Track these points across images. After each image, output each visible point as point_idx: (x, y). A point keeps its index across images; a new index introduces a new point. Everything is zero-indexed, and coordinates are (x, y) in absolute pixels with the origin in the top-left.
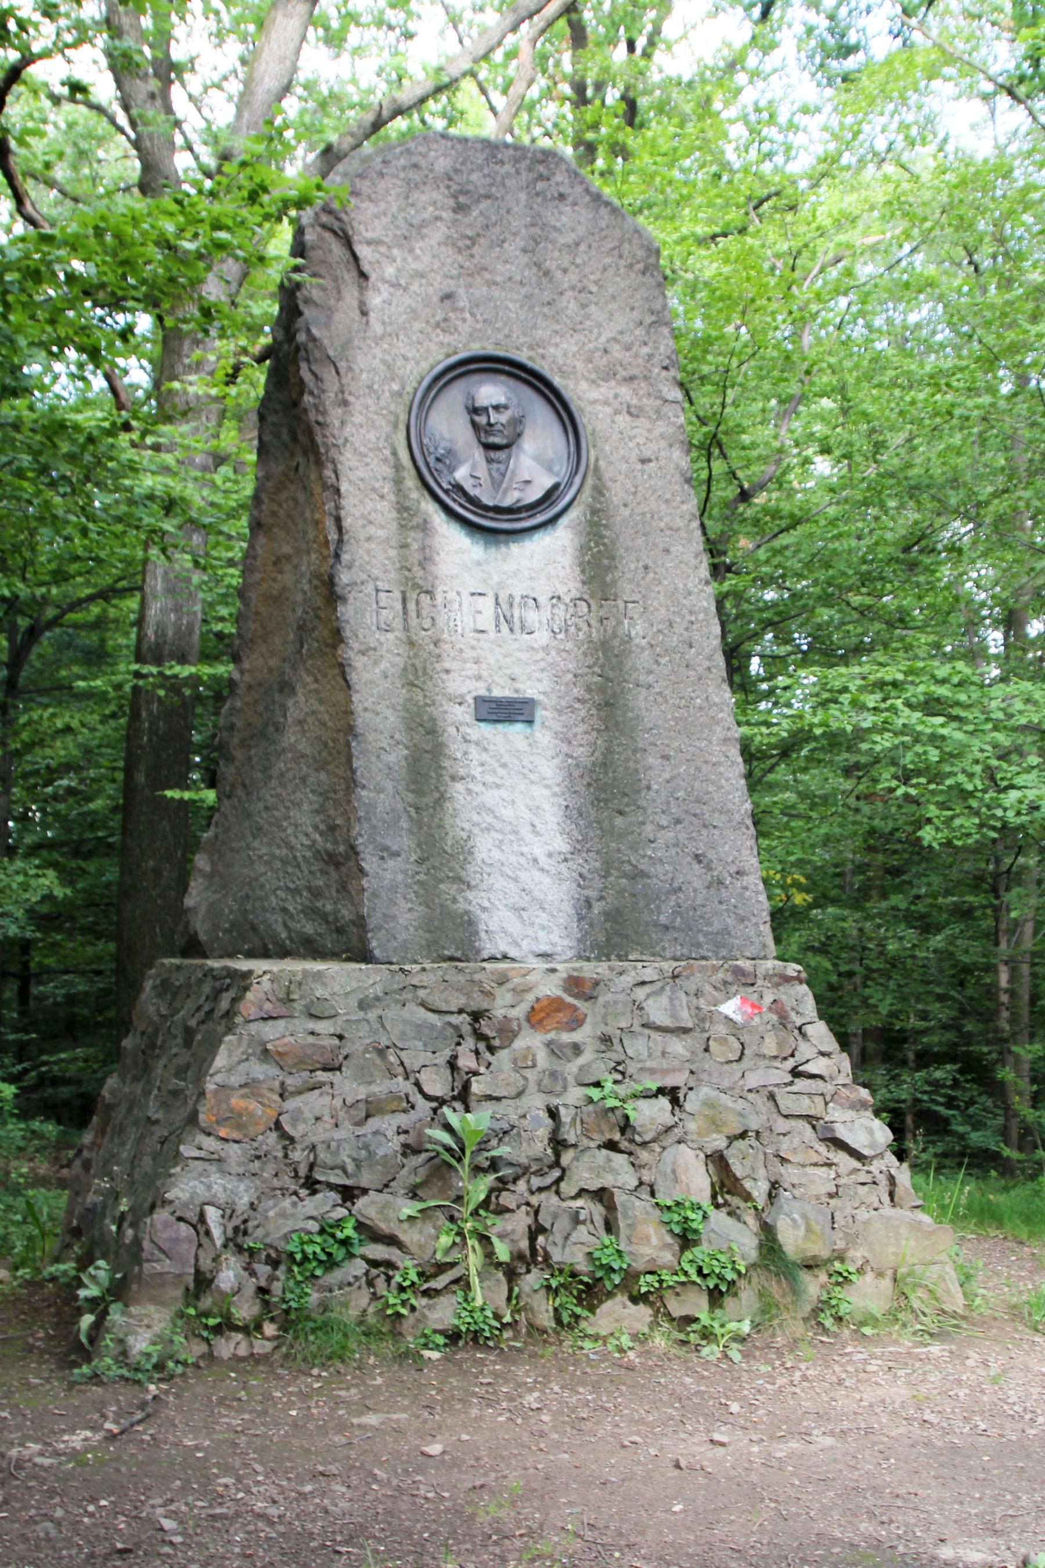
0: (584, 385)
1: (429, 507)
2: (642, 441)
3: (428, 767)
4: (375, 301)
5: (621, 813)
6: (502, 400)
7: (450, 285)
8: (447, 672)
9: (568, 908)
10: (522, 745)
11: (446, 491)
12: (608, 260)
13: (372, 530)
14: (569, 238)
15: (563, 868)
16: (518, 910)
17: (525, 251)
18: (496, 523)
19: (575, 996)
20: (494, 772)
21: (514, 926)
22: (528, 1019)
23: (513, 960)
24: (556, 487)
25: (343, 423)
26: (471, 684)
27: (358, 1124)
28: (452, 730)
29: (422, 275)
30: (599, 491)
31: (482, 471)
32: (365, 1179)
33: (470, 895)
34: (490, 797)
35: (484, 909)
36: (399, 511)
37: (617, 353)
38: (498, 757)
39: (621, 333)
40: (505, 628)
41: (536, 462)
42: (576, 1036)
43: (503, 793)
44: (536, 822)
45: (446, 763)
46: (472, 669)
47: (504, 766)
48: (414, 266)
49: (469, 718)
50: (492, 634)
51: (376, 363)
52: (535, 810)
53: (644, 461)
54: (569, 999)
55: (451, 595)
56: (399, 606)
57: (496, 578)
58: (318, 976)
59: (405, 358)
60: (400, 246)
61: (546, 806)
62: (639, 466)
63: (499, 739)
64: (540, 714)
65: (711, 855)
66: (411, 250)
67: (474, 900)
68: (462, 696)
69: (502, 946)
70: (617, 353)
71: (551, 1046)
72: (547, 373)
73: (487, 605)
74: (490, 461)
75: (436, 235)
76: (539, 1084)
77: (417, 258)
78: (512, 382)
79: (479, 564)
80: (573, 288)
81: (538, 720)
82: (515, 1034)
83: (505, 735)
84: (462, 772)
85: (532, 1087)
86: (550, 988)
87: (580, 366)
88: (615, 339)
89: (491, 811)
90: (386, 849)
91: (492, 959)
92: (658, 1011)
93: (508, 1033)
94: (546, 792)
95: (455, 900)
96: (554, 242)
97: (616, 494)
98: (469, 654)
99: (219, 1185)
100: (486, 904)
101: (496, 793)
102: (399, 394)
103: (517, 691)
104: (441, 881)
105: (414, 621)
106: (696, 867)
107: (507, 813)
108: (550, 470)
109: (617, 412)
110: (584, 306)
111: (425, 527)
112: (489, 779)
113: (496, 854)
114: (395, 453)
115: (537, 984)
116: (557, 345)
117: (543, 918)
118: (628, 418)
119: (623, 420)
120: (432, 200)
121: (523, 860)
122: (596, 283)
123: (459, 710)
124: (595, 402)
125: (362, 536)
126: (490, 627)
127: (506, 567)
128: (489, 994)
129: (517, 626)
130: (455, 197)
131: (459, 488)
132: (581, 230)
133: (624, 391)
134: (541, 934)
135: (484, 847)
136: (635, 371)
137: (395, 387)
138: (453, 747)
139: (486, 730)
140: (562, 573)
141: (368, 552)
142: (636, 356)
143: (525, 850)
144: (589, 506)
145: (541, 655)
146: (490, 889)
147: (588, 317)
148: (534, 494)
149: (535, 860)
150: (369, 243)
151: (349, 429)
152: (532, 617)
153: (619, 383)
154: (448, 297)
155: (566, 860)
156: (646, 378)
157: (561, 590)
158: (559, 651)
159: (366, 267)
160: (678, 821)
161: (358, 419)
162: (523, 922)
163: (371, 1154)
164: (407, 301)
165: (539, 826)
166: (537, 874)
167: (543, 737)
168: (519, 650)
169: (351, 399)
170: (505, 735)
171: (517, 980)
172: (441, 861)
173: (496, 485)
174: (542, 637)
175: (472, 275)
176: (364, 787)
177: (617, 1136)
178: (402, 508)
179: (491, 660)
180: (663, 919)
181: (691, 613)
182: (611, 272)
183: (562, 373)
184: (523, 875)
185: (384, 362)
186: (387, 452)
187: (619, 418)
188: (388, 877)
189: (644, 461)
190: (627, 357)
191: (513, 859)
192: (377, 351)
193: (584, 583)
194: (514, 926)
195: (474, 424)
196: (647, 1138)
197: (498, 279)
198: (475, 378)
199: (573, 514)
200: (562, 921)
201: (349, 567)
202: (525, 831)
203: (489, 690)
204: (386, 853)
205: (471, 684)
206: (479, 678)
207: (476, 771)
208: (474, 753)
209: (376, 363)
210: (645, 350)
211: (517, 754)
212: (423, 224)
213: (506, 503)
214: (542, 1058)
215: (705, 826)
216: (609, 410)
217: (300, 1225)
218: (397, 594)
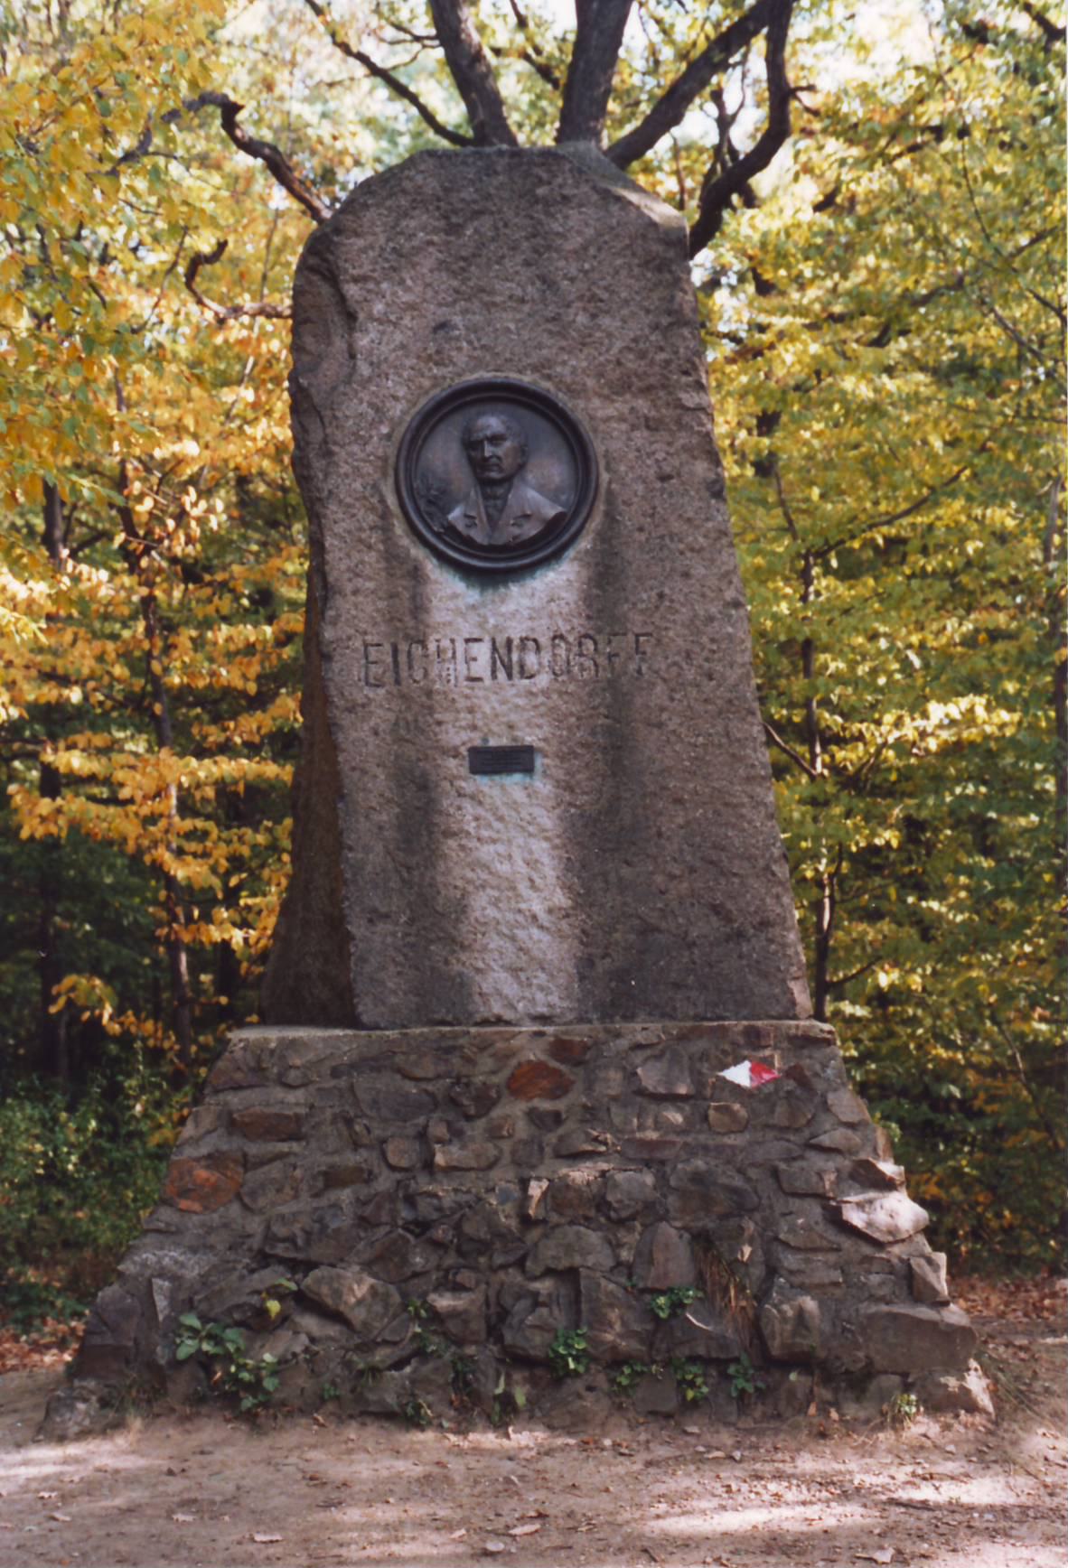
0: (596, 402)
1: (418, 552)
2: (660, 456)
3: (421, 823)
4: (363, 341)
5: (628, 863)
7: (443, 313)
8: (439, 723)
9: (570, 967)
10: (519, 795)
11: (438, 535)
12: (619, 262)
13: (359, 582)
14: (575, 242)
15: (564, 925)
16: (515, 971)
17: (527, 263)
18: (494, 565)
19: (562, 1061)
20: (490, 826)
21: (510, 988)
22: (508, 1086)
23: (508, 1023)
25: (326, 475)
26: (464, 736)
27: (316, 1195)
28: (446, 785)
29: (412, 307)
31: (479, 511)
32: (315, 1253)
33: (463, 957)
34: (486, 852)
35: (478, 971)
36: (387, 560)
37: (631, 363)
38: (494, 810)
39: (635, 340)
40: (502, 675)
41: (537, 496)
42: (560, 1105)
43: (501, 848)
44: (535, 876)
45: (437, 819)
46: (465, 718)
47: (501, 819)
48: (406, 298)
49: (464, 771)
50: (488, 682)
51: (364, 407)
52: (532, 863)
53: (664, 478)
54: (554, 1064)
55: (446, 643)
56: (389, 660)
57: (492, 621)
58: (293, 1043)
59: (395, 398)
60: (390, 279)
61: (546, 860)
62: (658, 485)
63: (496, 792)
64: (539, 762)
65: (730, 905)
66: (402, 282)
67: (463, 963)
68: (456, 748)
69: (497, 1008)
70: (631, 363)
71: (533, 1116)
73: (482, 651)
74: (486, 497)
75: (427, 263)
76: (513, 1153)
77: (408, 290)
79: (473, 607)
80: (581, 298)
82: (494, 1103)
83: (503, 787)
84: (455, 827)
85: (507, 1158)
86: (535, 1053)
87: (590, 382)
88: (629, 349)
89: (486, 867)
90: (375, 911)
91: (485, 1022)
92: (650, 1076)
93: (485, 1101)
94: (545, 845)
95: (447, 962)
96: (558, 250)
97: (630, 518)
99: (171, 1256)
100: (480, 965)
101: (492, 848)
102: (389, 437)
104: (432, 942)
105: (404, 674)
106: (714, 919)
107: (504, 868)
108: (555, 499)
109: (634, 427)
110: (594, 316)
111: (416, 574)
112: (485, 833)
113: (491, 912)
114: (382, 501)
115: (522, 1048)
116: (564, 363)
117: (542, 978)
118: (646, 433)
120: (420, 225)
121: (520, 918)
122: (606, 289)
123: (452, 763)
124: (608, 419)
125: (349, 587)
126: (486, 674)
127: (503, 609)
128: (470, 1061)
129: (516, 669)
130: (446, 218)
131: (451, 529)
132: (590, 232)
133: (642, 405)
134: (540, 996)
135: (481, 906)
136: (652, 380)
137: (385, 430)
138: (445, 803)
139: (483, 783)
140: (565, 610)
141: (356, 606)
142: (652, 363)
143: (523, 906)
145: (541, 699)
146: (485, 949)
148: (531, 530)
149: (534, 917)
150: (356, 280)
151: (332, 481)
152: (531, 659)
153: (635, 396)
154: (443, 326)
155: (567, 916)
156: (664, 387)
157: (564, 628)
158: (561, 693)
159: (353, 306)
160: (692, 870)
161: (345, 468)
162: (520, 983)
163: (324, 1228)
164: (398, 337)
165: (538, 881)
166: (535, 932)
167: (543, 786)
168: (518, 695)
169: (336, 449)
170: (503, 787)
171: (500, 1045)
172: (435, 921)
173: (493, 522)
174: (543, 680)
175: (468, 300)
176: (351, 849)
177: (592, 1213)
178: (392, 556)
179: (487, 710)
181: (713, 640)
182: (624, 273)
183: (571, 391)
184: (520, 934)
185: (371, 404)
186: (374, 500)
187: (637, 434)
188: (375, 941)
189: (664, 478)
190: (641, 366)
191: (510, 916)
192: (365, 396)
193: (589, 617)
194: (510, 988)
196: (624, 1214)
197: (498, 299)
200: (562, 980)
201: (334, 623)
202: (523, 888)
203: (485, 740)
204: (375, 917)
205: (464, 736)
206: (474, 728)
207: (471, 827)
208: (469, 807)
209: (364, 407)
210: (662, 356)
211: (515, 806)
212: (417, 250)
214: (522, 1129)
215: (723, 874)
216: (624, 427)
217: (244, 1299)
218: (387, 647)
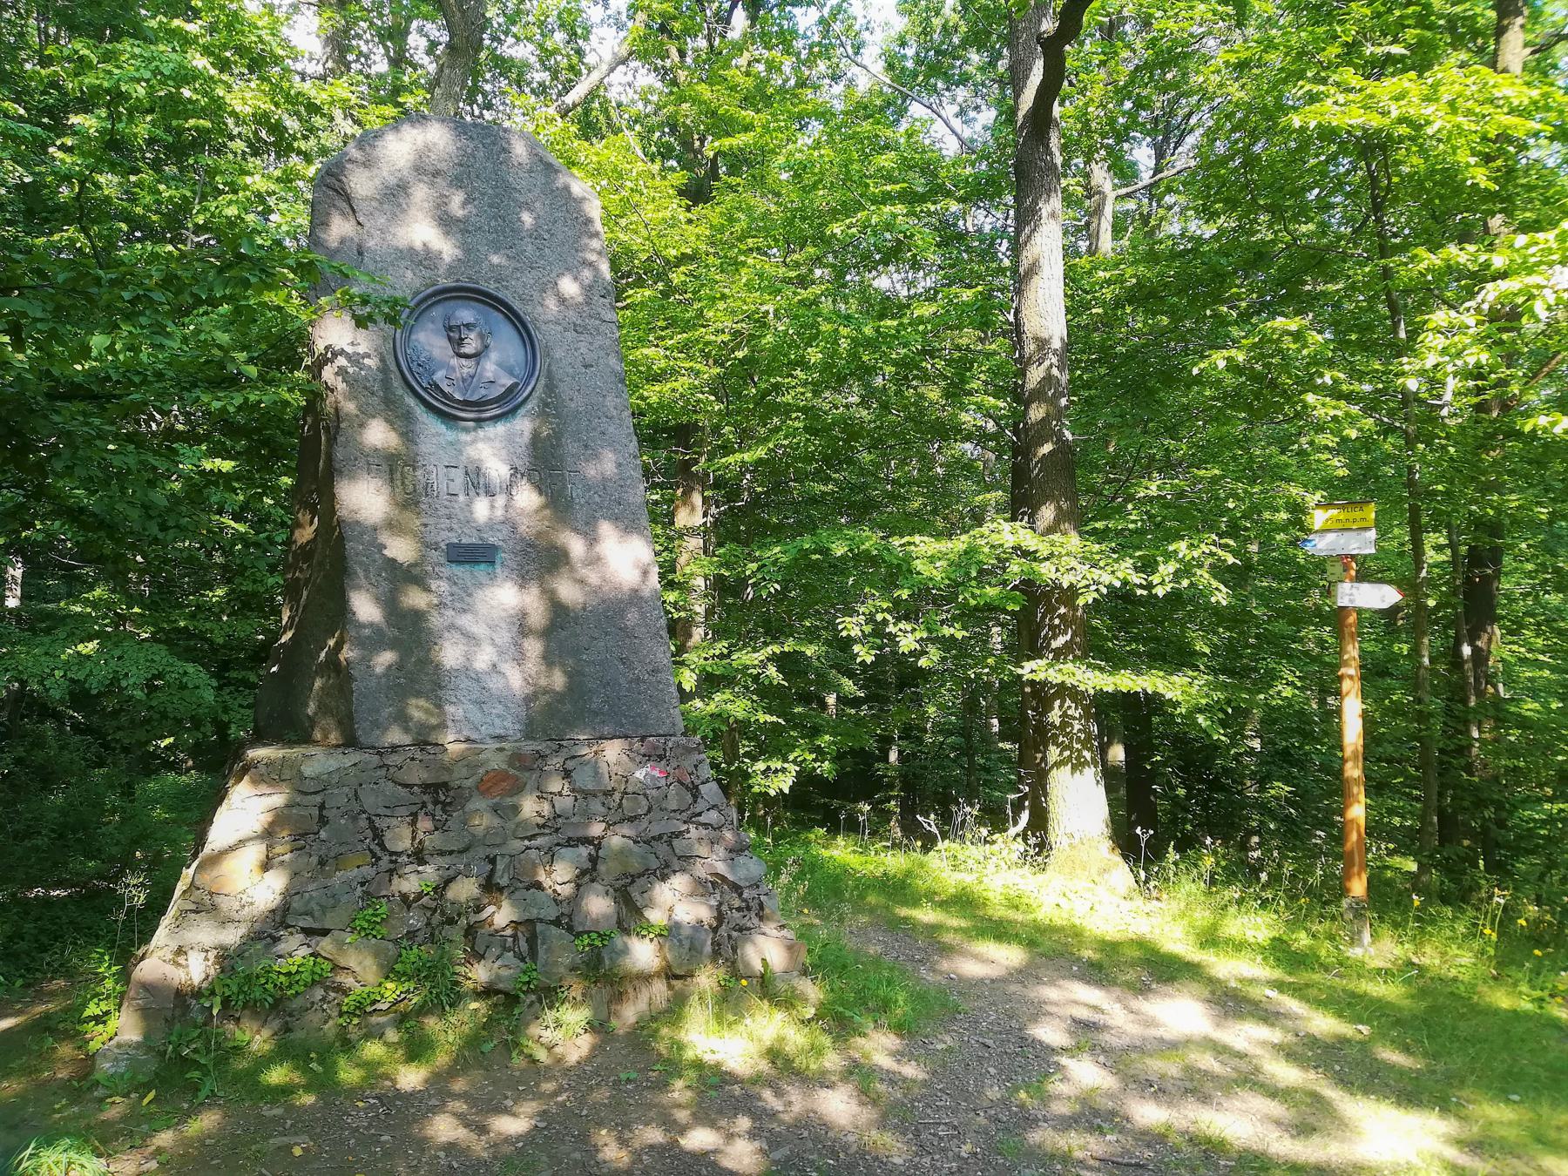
1: (411, 401)
6: (472, 320)
11: (425, 389)
24: (516, 385)
26: (445, 534)
30: (551, 388)
49: (443, 560)
54: (512, 771)
72: (510, 300)
78: (481, 306)
81: (498, 561)
98: (443, 511)
103: (1356, 757)
108: (511, 373)
109: (566, 330)
119: (571, 335)
122: (548, 231)
134: (497, 721)
144: (541, 399)
147: (542, 257)
148: (496, 392)
180: (594, 706)
195: (450, 339)
198: (452, 303)
199: (529, 406)
205: (445, 534)
206: (451, 529)
213: (475, 398)
216: (559, 328)
